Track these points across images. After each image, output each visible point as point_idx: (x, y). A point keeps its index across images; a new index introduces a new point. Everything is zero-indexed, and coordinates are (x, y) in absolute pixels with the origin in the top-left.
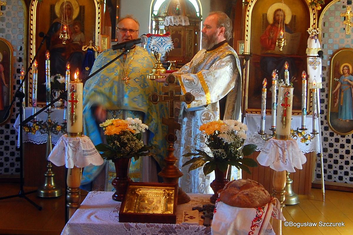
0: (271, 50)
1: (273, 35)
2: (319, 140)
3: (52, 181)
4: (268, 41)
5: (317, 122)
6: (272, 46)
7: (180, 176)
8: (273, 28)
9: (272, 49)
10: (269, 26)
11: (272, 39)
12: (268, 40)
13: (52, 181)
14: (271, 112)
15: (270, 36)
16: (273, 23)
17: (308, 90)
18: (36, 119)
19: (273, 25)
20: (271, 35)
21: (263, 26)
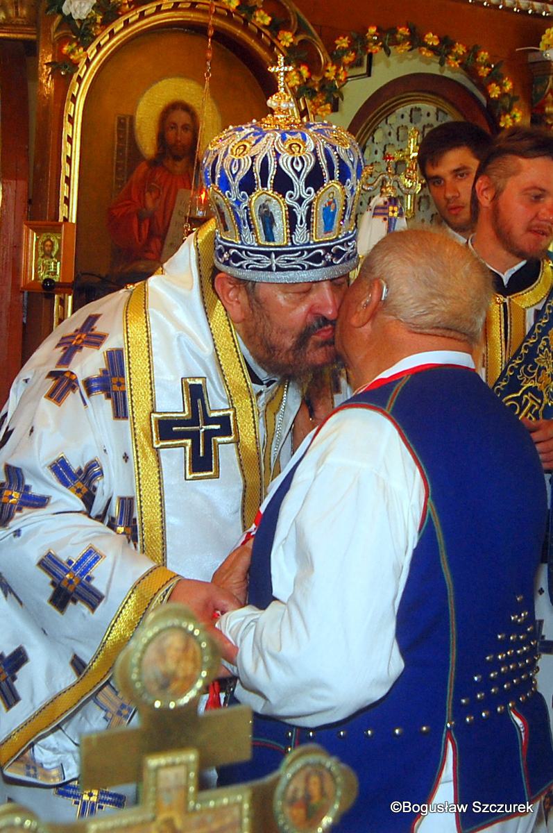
0: (147, 259)
1: (154, 201)
2: (170, 298)
3: (448, 771)
4: (135, 226)
5: (360, 390)
6: (152, 245)
7: (219, 780)
8: (158, 176)
9: (149, 255)
10: (143, 168)
11: (152, 218)
12: (136, 220)
13: (448, 771)
14: (102, 521)
15: (145, 206)
16: (157, 155)
17: (267, 244)
18: (140, 680)
19: (155, 163)
20: (149, 203)
21: (118, 165)
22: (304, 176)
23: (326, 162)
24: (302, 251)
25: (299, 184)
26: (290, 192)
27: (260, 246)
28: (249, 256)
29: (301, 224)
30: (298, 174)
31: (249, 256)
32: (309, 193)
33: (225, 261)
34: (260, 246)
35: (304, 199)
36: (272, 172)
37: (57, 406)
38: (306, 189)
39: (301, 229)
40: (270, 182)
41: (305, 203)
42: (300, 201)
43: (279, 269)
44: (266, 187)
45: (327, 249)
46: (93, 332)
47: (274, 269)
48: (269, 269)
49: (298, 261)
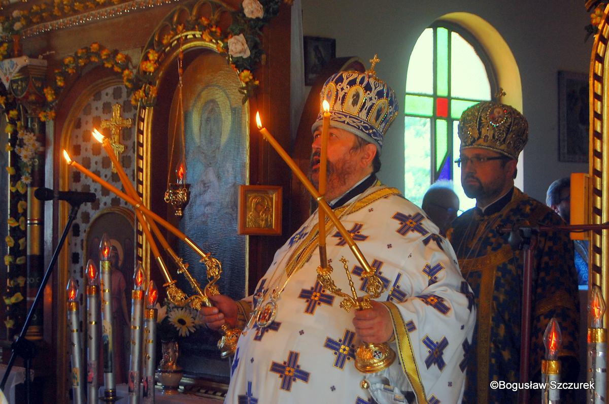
22: (349, 79)
23: (333, 76)
24: (361, 122)
25: (346, 82)
26: (341, 83)
27: (342, 112)
28: (358, 126)
29: (365, 110)
30: (376, 88)
31: (358, 126)
32: (347, 87)
33: (373, 129)
34: (342, 112)
35: (372, 99)
36: (365, 83)
37: (282, 324)
38: (146, 49)
39: (364, 112)
40: (364, 85)
41: (344, 91)
42: (342, 89)
43: (348, 124)
44: (362, 85)
45: (372, 128)
46: (359, 234)
47: (346, 123)
48: (344, 122)
49: (359, 124)
